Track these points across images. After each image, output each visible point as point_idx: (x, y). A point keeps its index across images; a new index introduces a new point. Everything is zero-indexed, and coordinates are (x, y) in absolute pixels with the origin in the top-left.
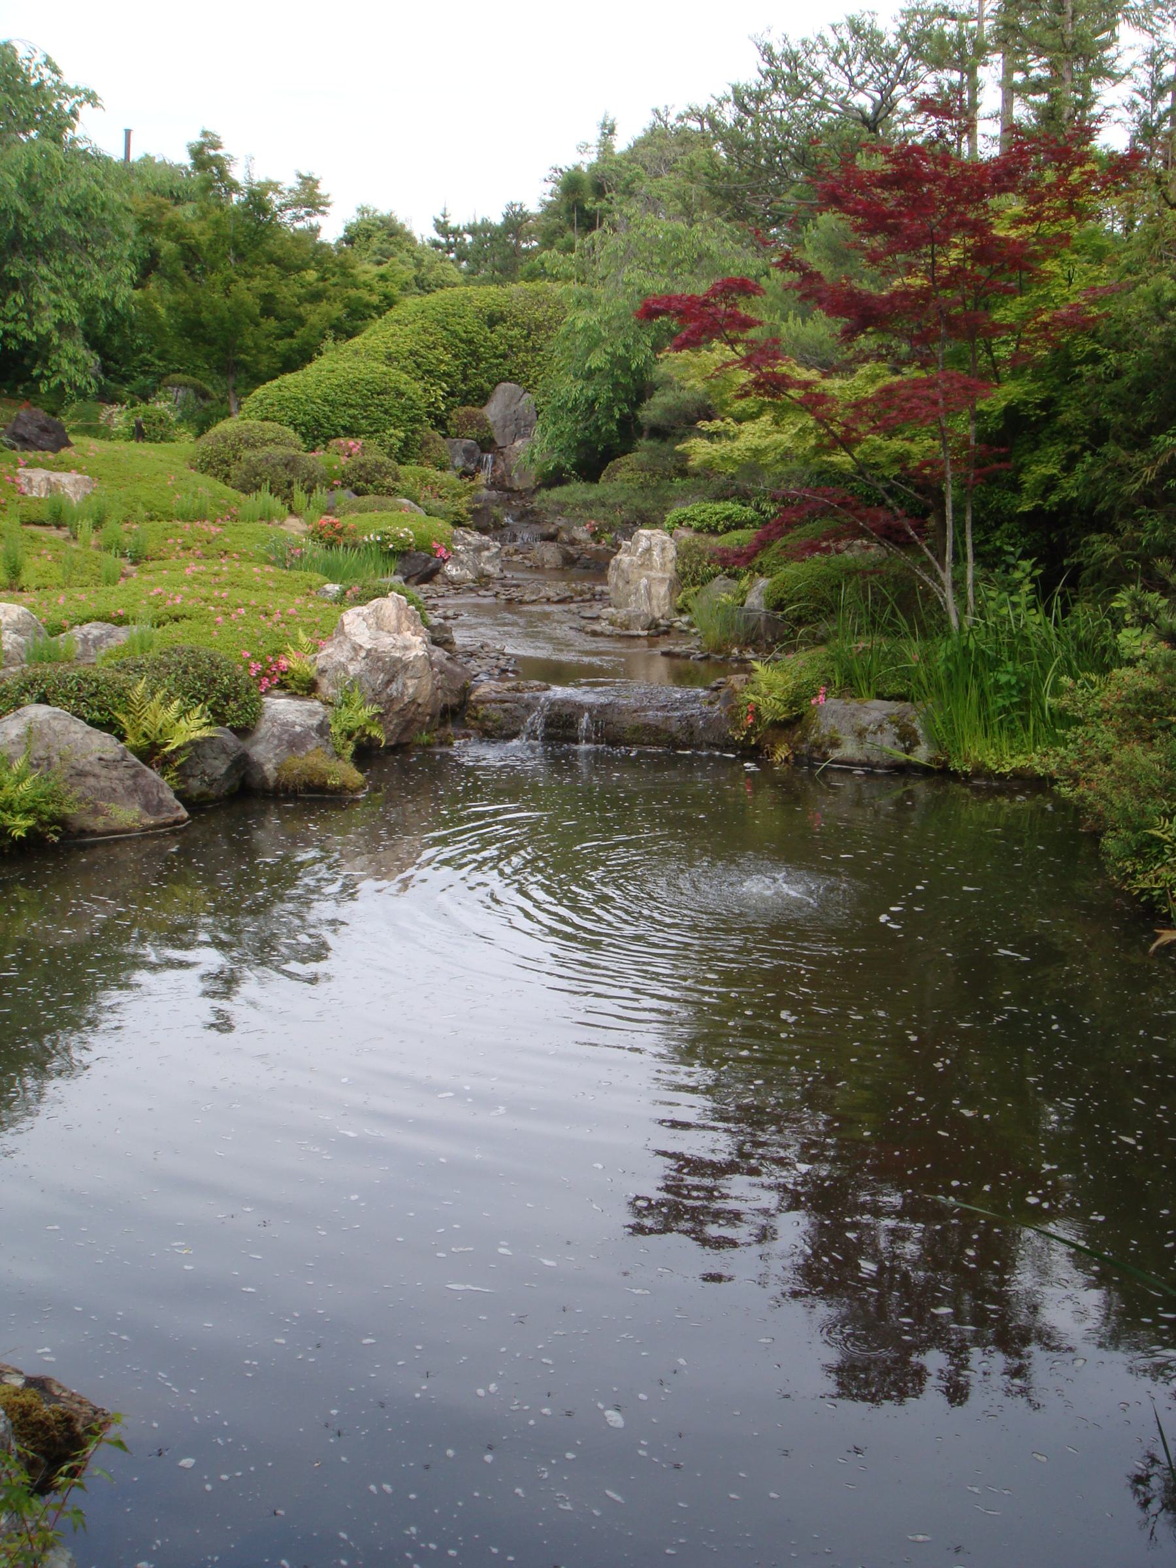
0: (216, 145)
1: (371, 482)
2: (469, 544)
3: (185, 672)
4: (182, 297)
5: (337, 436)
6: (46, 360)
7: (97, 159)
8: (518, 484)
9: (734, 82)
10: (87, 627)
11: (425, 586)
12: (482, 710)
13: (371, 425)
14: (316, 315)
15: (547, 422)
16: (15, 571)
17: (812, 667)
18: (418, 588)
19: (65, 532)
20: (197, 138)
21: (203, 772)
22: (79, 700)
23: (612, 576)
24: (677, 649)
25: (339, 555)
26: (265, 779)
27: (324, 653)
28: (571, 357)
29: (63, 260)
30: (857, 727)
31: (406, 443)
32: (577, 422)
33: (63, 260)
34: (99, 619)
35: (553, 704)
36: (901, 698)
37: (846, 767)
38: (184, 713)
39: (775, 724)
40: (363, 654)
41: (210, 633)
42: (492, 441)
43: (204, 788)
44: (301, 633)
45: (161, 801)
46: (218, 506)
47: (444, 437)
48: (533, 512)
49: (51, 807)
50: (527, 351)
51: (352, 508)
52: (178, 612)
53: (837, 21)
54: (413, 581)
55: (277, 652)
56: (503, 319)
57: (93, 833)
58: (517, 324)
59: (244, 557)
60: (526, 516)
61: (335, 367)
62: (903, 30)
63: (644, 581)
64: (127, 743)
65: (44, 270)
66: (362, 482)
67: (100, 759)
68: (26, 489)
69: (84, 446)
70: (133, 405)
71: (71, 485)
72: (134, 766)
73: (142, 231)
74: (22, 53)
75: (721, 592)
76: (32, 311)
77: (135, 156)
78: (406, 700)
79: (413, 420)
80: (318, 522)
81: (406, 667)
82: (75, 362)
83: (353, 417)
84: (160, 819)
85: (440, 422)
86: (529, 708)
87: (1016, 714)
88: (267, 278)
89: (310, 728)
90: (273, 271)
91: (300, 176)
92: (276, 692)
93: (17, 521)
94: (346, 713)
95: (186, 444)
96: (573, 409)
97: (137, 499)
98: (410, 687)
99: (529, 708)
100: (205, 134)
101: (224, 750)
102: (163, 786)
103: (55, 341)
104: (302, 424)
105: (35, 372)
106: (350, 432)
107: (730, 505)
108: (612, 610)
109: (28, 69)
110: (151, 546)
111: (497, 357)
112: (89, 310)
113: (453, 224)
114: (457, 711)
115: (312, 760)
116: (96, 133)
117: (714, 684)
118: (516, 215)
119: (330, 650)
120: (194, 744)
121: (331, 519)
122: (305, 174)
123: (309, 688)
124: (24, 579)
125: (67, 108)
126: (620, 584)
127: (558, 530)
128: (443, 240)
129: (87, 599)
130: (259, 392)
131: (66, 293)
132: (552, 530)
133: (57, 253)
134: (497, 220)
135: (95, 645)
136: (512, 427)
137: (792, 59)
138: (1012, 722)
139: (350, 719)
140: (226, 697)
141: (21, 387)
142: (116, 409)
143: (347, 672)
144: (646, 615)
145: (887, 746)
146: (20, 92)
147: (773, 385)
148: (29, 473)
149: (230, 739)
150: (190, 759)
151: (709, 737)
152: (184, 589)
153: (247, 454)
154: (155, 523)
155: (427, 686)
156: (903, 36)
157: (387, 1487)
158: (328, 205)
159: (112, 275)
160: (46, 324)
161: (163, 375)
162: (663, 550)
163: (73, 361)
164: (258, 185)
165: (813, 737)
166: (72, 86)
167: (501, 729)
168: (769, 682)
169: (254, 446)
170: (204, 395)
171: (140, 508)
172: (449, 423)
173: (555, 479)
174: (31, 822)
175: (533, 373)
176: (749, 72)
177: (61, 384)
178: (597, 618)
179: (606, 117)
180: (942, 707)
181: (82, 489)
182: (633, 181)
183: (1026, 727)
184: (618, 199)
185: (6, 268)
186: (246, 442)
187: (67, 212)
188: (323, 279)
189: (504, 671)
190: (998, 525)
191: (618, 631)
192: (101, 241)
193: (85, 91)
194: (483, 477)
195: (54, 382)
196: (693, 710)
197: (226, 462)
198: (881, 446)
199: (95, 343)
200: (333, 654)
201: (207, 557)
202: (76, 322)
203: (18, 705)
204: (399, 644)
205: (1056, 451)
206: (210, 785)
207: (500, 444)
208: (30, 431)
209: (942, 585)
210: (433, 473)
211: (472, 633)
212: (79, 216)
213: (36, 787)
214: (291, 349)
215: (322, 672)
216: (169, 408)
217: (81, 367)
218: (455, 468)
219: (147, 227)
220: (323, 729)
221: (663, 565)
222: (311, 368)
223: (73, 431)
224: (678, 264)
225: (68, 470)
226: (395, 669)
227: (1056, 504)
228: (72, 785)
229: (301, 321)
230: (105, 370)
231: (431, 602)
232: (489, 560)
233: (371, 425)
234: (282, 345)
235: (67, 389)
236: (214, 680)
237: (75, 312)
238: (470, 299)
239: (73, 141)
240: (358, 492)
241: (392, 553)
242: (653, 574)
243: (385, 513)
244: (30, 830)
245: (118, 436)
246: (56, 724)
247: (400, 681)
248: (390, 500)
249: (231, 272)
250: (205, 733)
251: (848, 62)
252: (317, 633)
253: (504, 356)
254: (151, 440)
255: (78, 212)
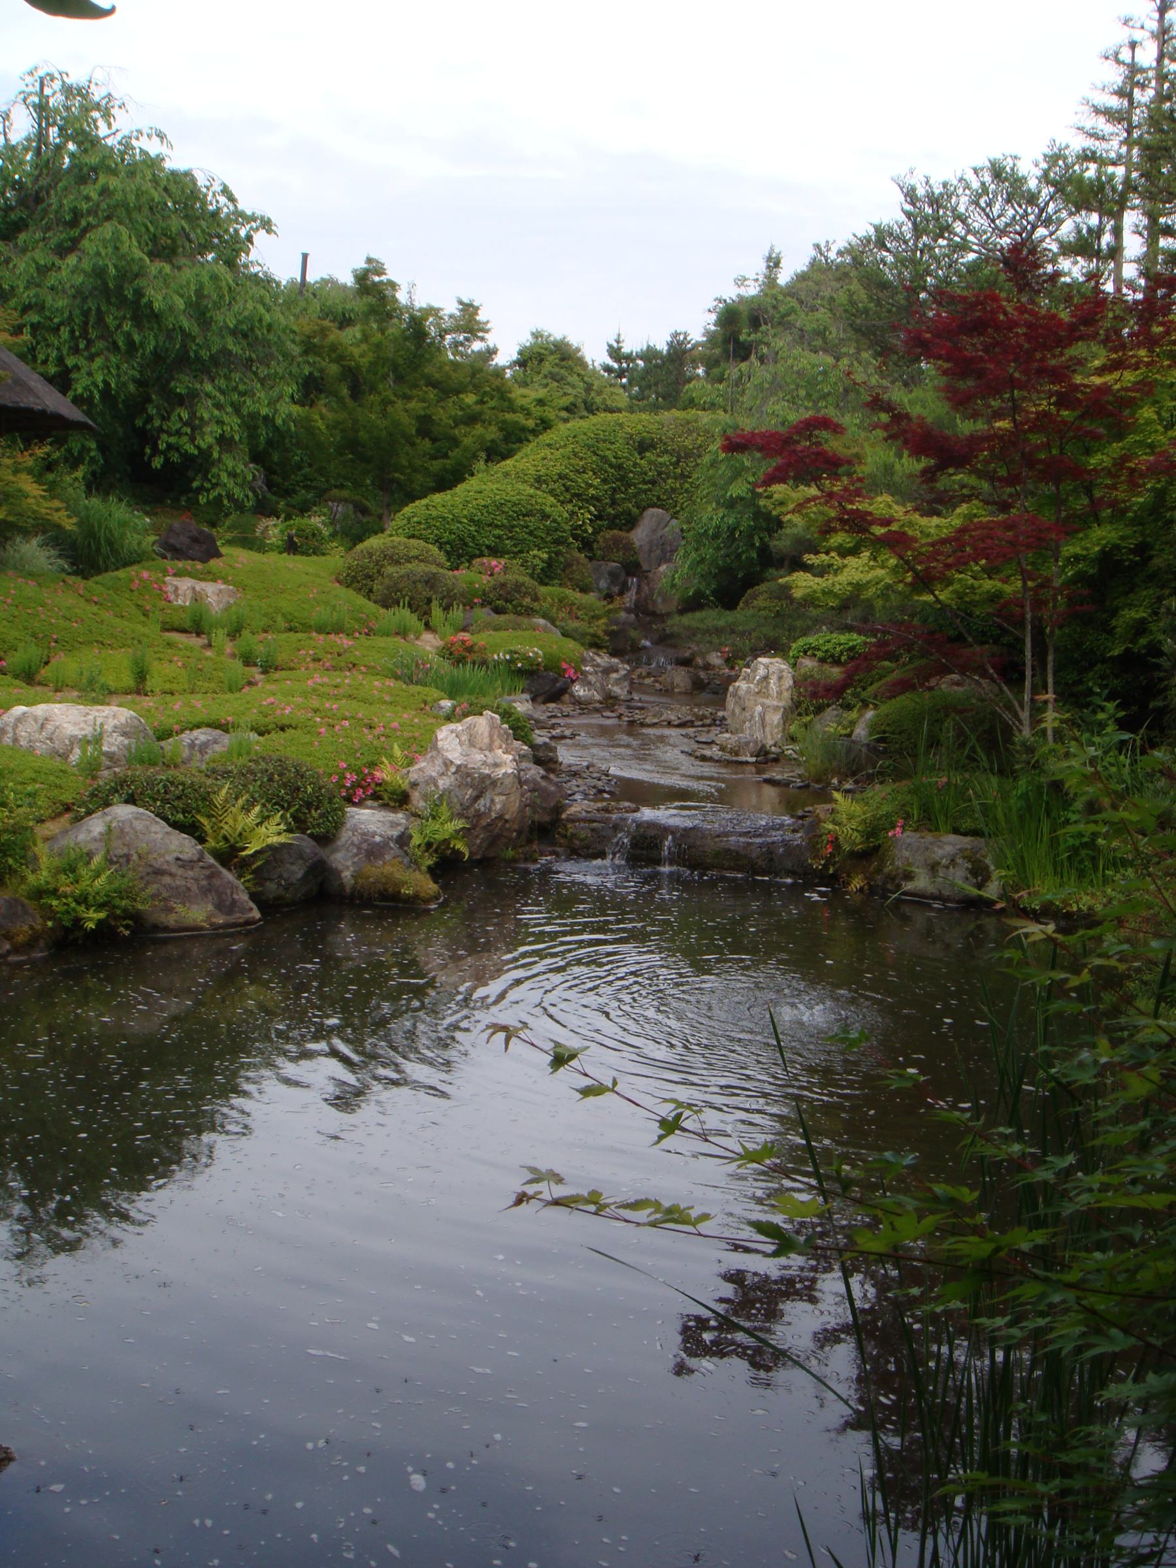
0: (380, 271)
1: (511, 601)
2: (598, 665)
3: (271, 780)
4: (343, 416)
5: (482, 555)
6: (207, 472)
7: (266, 282)
8: (661, 608)
9: (877, 222)
10: (196, 733)
11: (552, 705)
12: (571, 829)
13: (515, 545)
14: (470, 437)
15: (689, 548)
16: (141, 676)
17: (894, 799)
18: (544, 707)
19: (203, 640)
20: (362, 265)
21: (281, 877)
22: (165, 801)
23: (730, 703)
24: (779, 777)
25: (466, 672)
26: (342, 885)
27: (417, 767)
28: (715, 485)
29: (227, 378)
30: (930, 860)
31: (550, 563)
32: (719, 549)
33: (227, 378)
34: (209, 725)
35: (639, 825)
36: (975, 833)
37: (921, 900)
38: (264, 819)
39: (853, 855)
40: (453, 769)
41: (311, 744)
42: (638, 565)
43: (281, 892)
44: (396, 747)
45: (234, 902)
46: (358, 620)
47: (590, 559)
48: (672, 636)
49: (124, 903)
50: (675, 478)
51: (488, 626)
52: (286, 722)
53: (980, 165)
54: (540, 699)
55: (373, 765)
56: (652, 446)
57: (166, 929)
58: (666, 452)
59: (371, 670)
60: (665, 640)
61: (486, 487)
62: (1046, 173)
63: (759, 708)
64: (207, 845)
65: (209, 387)
66: (504, 602)
67: (178, 859)
68: (172, 597)
69: (237, 557)
70: (288, 517)
71: (214, 595)
72: (211, 866)
73: (306, 353)
74: (201, 182)
75: (830, 723)
76: (195, 426)
77: (310, 278)
78: (494, 815)
79: (557, 542)
80: (450, 638)
81: (494, 783)
82: (235, 474)
83: (499, 537)
84: (232, 919)
85: (587, 545)
86: (616, 828)
87: (1083, 853)
88: (424, 401)
89: (390, 838)
90: (432, 394)
91: (461, 303)
92: (369, 803)
93: (159, 627)
94: (433, 826)
95: (337, 558)
96: (716, 536)
97: (278, 610)
98: (497, 803)
99: (616, 828)
100: (369, 260)
101: (301, 856)
102: (238, 887)
103: (216, 455)
104: (447, 543)
105: (195, 484)
106: (495, 552)
107: (855, 636)
108: (727, 735)
109: (206, 196)
110: (282, 657)
111: (646, 483)
112: (251, 423)
113: (626, 349)
114: (546, 828)
115: (388, 869)
116: (273, 258)
117: (800, 813)
118: (680, 343)
119: (423, 764)
120: (270, 847)
121: (465, 636)
122: (466, 301)
123: (400, 800)
124: (149, 684)
125: (243, 233)
126: (737, 711)
127: (693, 655)
128: (616, 366)
129: (202, 706)
130: (408, 510)
131: (229, 409)
132: (687, 654)
133: (223, 371)
134: (662, 346)
135: (198, 748)
136: (658, 552)
137: (935, 201)
138: (1081, 862)
139: (435, 832)
140: (309, 805)
141: (183, 498)
142: (272, 521)
143: (436, 786)
144: (756, 742)
145: (959, 880)
146: (198, 218)
147: (858, 523)
148: (176, 581)
149: (308, 845)
150: (267, 862)
151: (789, 864)
152: (298, 700)
153: (390, 569)
154: (292, 634)
155: (515, 803)
156: (1045, 178)
157: (209, 1523)
158: (487, 331)
159: (274, 393)
160: (207, 439)
161: (325, 491)
162: (780, 678)
163: (233, 475)
164: (420, 310)
165: (888, 869)
166: (249, 213)
167: (588, 847)
168: (847, 813)
169: (398, 563)
170: (364, 511)
171: (279, 619)
172: (595, 546)
173: (693, 604)
174: (102, 915)
175: (681, 499)
176: (890, 211)
177: (220, 495)
178: (710, 743)
179: (772, 250)
180: (1013, 845)
181: (226, 599)
182: (788, 314)
183: (1095, 868)
184: (772, 332)
185: (172, 384)
186: (391, 557)
187: (234, 332)
188: (482, 402)
189: (601, 791)
190: (1092, 666)
191: (728, 757)
192: (266, 361)
193: (262, 218)
194: (630, 598)
195: (213, 494)
196: (776, 836)
197: (368, 577)
198: (977, 582)
199: (257, 457)
200: (425, 767)
201: (334, 668)
202: (237, 438)
203: (107, 804)
204: (490, 761)
205: (1147, 593)
206: (286, 889)
207: (645, 567)
208: (182, 541)
209: (1020, 722)
210: (575, 595)
211: (585, 753)
212: (245, 336)
213: (110, 883)
214: (445, 470)
215: (414, 785)
216: (323, 523)
217: (240, 480)
218: (599, 590)
219: (309, 348)
220: (403, 840)
221: (780, 693)
222: (460, 488)
223: (229, 542)
224: (824, 397)
225: (214, 580)
226: (483, 785)
227: (1145, 647)
228: (148, 883)
229: (455, 442)
230: (270, 484)
231: (554, 721)
232: (617, 682)
233: (515, 545)
234: (436, 465)
235: (225, 502)
236: (298, 789)
237: (236, 428)
238: (621, 425)
239: (246, 266)
240: (498, 611)
241: (520, 672)
242: (767, 702)
243: (520, 633)
244: (100, 923)
245: (272, 548)
246: (139, 825)
247: (488, 795)
248: (524, 620)
249: (389, 393)
250: (282, 839)
251: (990, 204)
252: (415, 747)
253: (653, 482)
254: (303, 554)
255: (245, 332)
